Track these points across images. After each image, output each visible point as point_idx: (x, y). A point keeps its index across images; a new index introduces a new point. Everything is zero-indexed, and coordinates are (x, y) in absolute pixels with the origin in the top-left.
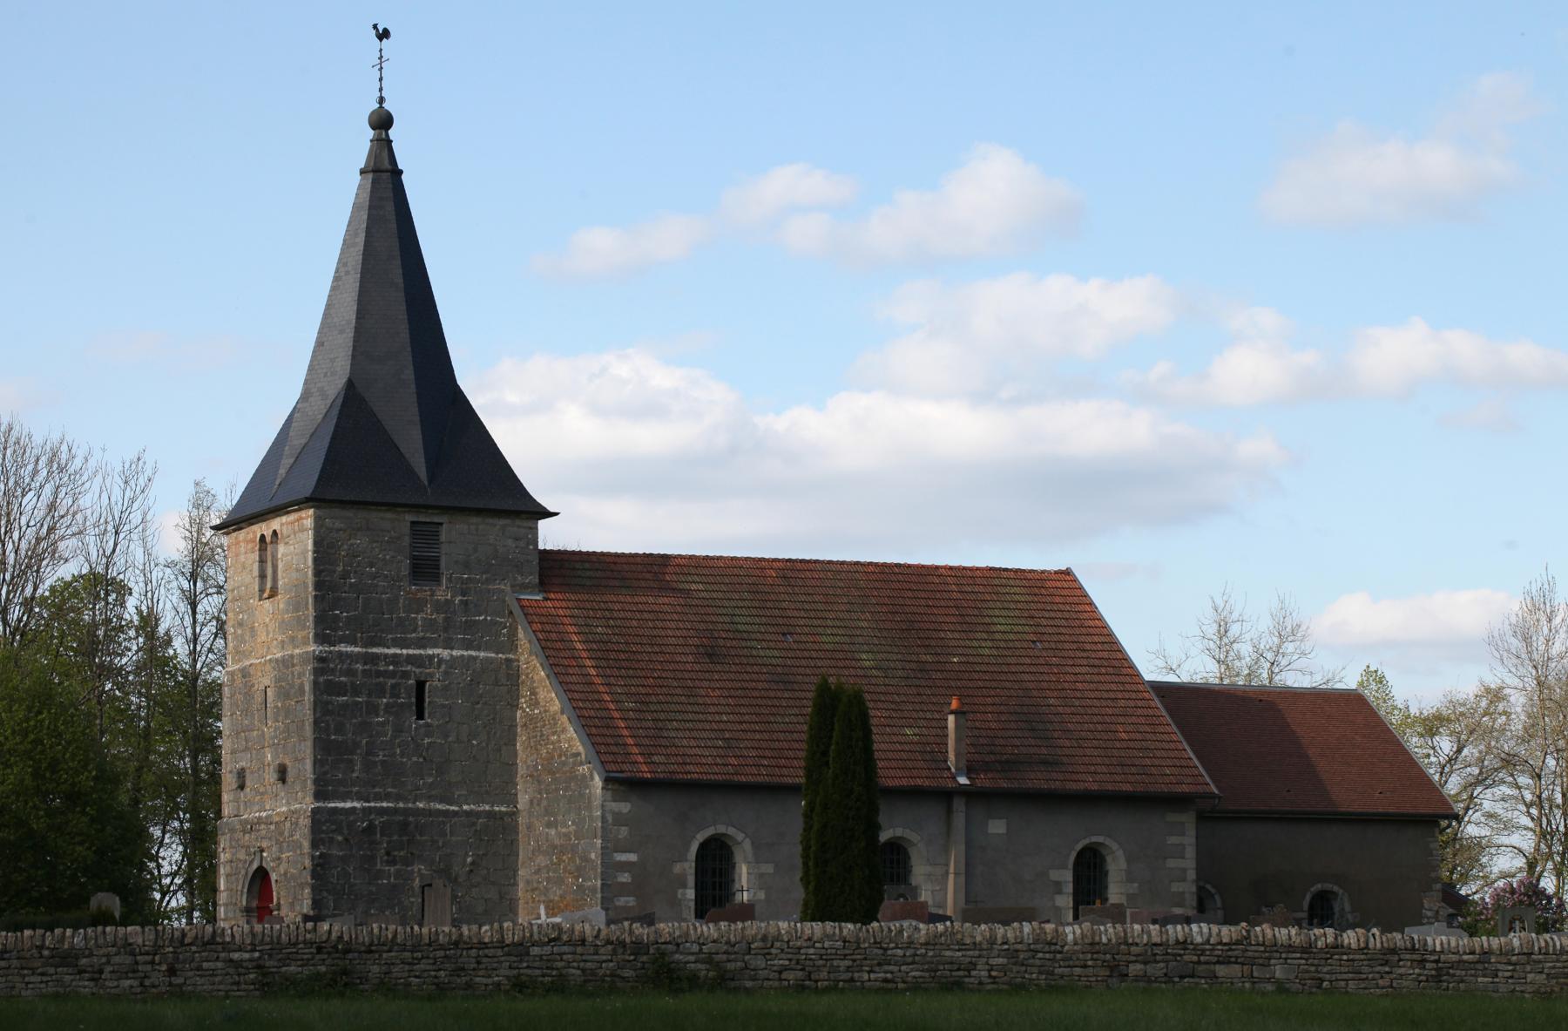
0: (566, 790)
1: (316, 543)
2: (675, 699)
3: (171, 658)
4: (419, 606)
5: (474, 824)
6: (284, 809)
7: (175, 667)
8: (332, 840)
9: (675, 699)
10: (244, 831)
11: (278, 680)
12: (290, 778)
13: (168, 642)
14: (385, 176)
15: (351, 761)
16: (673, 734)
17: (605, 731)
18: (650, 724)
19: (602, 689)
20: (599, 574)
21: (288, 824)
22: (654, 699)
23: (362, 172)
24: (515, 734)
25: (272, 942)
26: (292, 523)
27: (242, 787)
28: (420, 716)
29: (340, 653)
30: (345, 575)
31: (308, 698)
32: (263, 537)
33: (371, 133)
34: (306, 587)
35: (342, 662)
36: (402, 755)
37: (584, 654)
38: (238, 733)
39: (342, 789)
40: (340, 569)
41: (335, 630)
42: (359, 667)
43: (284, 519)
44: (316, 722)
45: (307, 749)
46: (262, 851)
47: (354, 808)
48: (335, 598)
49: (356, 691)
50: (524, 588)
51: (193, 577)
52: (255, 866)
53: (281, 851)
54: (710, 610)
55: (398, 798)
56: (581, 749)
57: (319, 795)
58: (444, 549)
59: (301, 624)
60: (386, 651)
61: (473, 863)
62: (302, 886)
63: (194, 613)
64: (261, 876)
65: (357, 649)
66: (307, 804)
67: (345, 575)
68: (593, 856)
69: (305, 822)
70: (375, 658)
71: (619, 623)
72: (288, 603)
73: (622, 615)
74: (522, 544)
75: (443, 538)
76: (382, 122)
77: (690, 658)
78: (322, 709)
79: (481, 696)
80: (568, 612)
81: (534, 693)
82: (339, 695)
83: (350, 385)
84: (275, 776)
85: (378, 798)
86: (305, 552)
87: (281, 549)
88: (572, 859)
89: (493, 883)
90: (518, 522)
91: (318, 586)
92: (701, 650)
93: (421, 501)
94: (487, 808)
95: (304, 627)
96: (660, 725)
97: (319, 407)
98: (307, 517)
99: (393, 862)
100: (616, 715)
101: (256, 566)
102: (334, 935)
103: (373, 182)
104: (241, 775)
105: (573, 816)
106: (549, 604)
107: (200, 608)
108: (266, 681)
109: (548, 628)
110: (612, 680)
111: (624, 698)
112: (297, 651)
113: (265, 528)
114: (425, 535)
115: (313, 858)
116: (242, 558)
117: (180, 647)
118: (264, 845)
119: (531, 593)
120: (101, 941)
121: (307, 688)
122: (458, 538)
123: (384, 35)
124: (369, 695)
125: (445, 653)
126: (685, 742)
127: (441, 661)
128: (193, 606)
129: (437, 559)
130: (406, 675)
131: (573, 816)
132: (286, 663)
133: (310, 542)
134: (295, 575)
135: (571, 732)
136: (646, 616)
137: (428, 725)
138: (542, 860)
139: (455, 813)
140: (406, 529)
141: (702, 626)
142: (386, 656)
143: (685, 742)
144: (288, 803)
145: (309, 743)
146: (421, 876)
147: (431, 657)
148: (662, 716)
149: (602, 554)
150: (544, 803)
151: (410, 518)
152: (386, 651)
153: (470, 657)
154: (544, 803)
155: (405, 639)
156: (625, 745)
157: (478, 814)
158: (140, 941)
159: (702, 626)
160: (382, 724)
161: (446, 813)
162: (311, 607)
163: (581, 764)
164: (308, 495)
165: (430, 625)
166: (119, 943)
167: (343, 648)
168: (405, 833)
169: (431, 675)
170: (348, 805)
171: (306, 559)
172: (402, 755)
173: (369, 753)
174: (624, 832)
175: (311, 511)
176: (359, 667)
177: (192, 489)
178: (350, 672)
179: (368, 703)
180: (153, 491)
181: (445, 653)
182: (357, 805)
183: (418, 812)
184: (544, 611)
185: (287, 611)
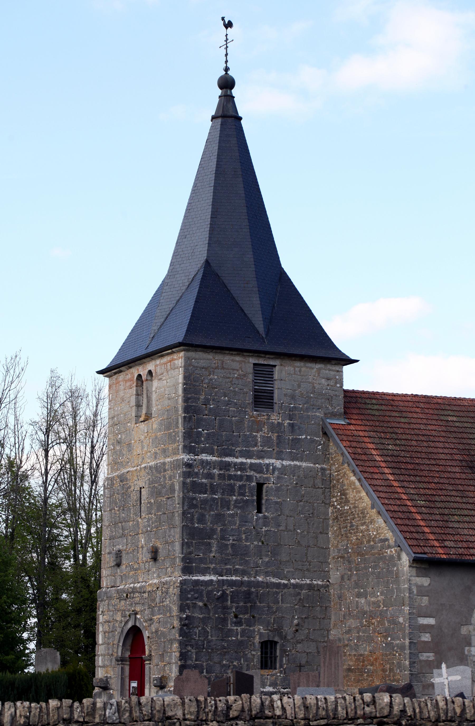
0: (374, 567)
1: (185, 378)
2: (453, 499)
3: (27, 488)
4: (258, 426)
5: (299, 594)
6: (156, 581)
7: (29, 494)
8: (195, 605)
9: (453, 499)
10: (120, 599)
11: (151, 482)
12: (161, 557)
13: (25, 477)
14: (230, 120)
15: (209, 544)
16: (456, 525)
17: (407, 522)
18: (438, 517)
19: (399, 490)
20: (383, 407)
21: (159, 593)
22: (437, 498)
23: (213, 118)
24: (328, 525)
25: (327, 717)
26: (165, 364)
27: (118, 565)
28: (259, 511)
29: (202, 461)
30: (206, 403)
31: (178, 494)
32: (140, 376)
33: (219, 92)
34: (177, 410)
35: (204, 468)
36: (247, 540)
37: (383, 465)
38: (116, 524)
39: (202, 566)
40: (202, 397)
41: (198, 443)
42: (216, 471)
43: (158, 362)
44: (184, 513)
45: (176, 535)
46: (136, 614)
47: (212, 581)
48: (199, 419)
49: (214, 492)
50: (334, 415)
51: (47, 433)
52: (130, 625)
53: (153, 614)
54: (465, 436)
55: (244, 573)
56: (389, 535)
57: (186, 570)
58: (277, 384)
59: (172, 438)
60: (236, 460)
61: (298, 625)
62: (171, 642)
63: (47, 456)
64: (134, 636)
65: (214, 458)
66: (177, 577)
67: (206, 403)
68: (401, 620)
69: (174, 591)
70: (227, 466)
71: (403, 442)
72: (161, 424)
73: (404, 437)
74: (332, 383)
75: (276, 376)
76: (227, 84)
77: (457, 469)
78: (189, 504)
79: (303, 496)
80: (366, 434)
81: (344, 493)
82: (200, 493)
83: (207, 263)
84: (149, 556)
85: (229, 572)
86: (175, 386)
87: (155, 384)
88: (381, 623)
89: (313, 640)
90: (329, 366)
91: (186, 409)
92: (464, 464)
93: (261, 349)
94: (308, 582)
95: (174, 441)
96: (446, 518)
97: (182, 281)
98: (179, 359)
99: (239, 623)
100: (413, 510)
101: (133, 399)
102: (396, 709)
103: (222, 125)
104: (119, 555)
105: (381, 588)
106: (352, 427)
107: (51, 453)
108: (141, 484)
109: (354, 444)
110: (405, 484)
111: (416, 497)
112: (168, 460)
113: (142, 370)
114: (263, 373)
115: (181, 619)
116: (121, 394)
117: (35, 482)
118: (138, 609)
119: (338, 419)
120: (136, 714)
121: (177, 487)
122: (288, 377)
123: (229, 25)
124: (223, 494)
125: (278, 463)
126: (466, 532)
127: (274, 469)
128: (47, 451)
129: (272, 392)
130: (249, 478)
131: (381, 588)
132: (159, 469)
133: (181, 379)
134: (166, 402)
135: (380, 521)
136: (421, 438)
137: (265, 517)
138: (352, 623)
139: (285, 586)
140: (250, 368)
141: (461, 447)
142: (235, 464)
143: (466, 532)
144: (159, 577)
145: (178, 530)
146: (261, 635)
147: (268, 465)
148: (446, 511)
149: (384, 394)
150: (354, 578)
151: (253, 360)
152: (236, 460)
153: (295, 465)
154: (354, 578)
155: (249, 451)
156: (424, 533)
157: (300, 587)
158: (179, 714)
159: (461, 447)
160: (232, 516)
161: (278, 585)
162: (180, 426)
163: (389, 547)
164: (180, 340)
165: (267, 441)
166: (158, 716)
167: (204, 457)
168: (248, 599)
169: (268, 479)
170: (207, 578)
171: (176, 390)
172: (247, 540)
173: (223, 538)
174: (425, 600)
175: (182, 354)
176: (216, 471)
177: (49, 374)
178: (210, 476)
179: (222, 499)
180: (24, 377)
181: (278, 463)
182: (214, 578)
183: (258, 585)
184: (348, 433)
185: (160, 430)
